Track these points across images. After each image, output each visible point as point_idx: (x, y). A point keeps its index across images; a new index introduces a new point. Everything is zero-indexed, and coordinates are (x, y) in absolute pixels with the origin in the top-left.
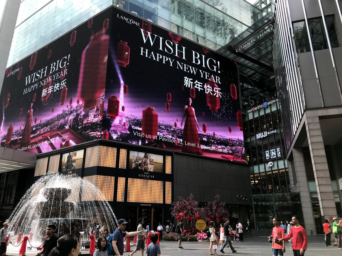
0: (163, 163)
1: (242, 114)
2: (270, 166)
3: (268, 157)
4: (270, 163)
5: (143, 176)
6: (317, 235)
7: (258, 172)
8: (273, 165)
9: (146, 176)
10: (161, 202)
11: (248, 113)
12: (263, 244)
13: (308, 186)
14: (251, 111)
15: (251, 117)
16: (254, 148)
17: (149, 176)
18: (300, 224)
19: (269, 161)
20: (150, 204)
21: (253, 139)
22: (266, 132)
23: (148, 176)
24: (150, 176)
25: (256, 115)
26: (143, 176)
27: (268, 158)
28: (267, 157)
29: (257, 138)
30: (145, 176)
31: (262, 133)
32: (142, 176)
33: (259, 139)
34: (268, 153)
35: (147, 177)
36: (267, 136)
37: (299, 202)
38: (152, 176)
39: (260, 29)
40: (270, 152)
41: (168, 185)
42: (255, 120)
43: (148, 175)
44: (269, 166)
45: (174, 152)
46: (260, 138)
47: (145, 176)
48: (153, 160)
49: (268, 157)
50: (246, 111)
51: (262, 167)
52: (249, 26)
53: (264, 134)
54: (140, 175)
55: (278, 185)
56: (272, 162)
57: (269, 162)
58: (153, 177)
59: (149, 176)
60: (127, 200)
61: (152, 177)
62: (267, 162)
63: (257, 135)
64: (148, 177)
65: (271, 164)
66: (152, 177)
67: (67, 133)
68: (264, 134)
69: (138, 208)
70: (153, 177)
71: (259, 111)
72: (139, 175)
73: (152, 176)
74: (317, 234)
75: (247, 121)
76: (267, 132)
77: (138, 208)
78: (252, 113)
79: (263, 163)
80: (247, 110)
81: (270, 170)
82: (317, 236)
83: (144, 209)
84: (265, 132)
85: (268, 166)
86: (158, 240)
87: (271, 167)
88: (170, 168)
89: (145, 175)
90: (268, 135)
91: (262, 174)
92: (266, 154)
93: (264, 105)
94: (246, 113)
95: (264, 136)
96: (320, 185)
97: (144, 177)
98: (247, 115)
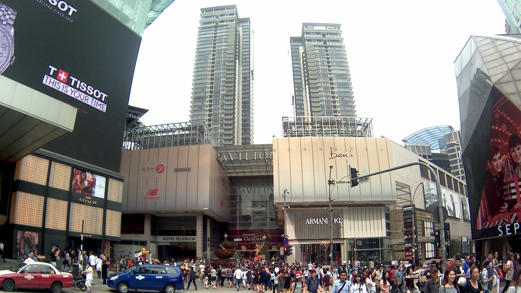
0: (73, 130)
5: (85, 201)
9: (88, 201)
10: (100, 232)
17: (90, 201)
18: (279, 229)
20: (90, 234)
23: (89, 201)
24: (91, 202)
26: (85, 201)
32: (83, 200)
38: (94, 202)
39: (240, 147)
47: (86, 201)
48: (451, 127)
52: (109, 199)
54: (81, 200)
58: (96, 204)
59: (90, 201)
60: (44, 226)
66: (94, 203)
70: (69, 19)
72: (80, 200)
73: (94, 202)
83: (254, 279)
86: (426, 283)
88: (45, 170)
97: (86, 202)
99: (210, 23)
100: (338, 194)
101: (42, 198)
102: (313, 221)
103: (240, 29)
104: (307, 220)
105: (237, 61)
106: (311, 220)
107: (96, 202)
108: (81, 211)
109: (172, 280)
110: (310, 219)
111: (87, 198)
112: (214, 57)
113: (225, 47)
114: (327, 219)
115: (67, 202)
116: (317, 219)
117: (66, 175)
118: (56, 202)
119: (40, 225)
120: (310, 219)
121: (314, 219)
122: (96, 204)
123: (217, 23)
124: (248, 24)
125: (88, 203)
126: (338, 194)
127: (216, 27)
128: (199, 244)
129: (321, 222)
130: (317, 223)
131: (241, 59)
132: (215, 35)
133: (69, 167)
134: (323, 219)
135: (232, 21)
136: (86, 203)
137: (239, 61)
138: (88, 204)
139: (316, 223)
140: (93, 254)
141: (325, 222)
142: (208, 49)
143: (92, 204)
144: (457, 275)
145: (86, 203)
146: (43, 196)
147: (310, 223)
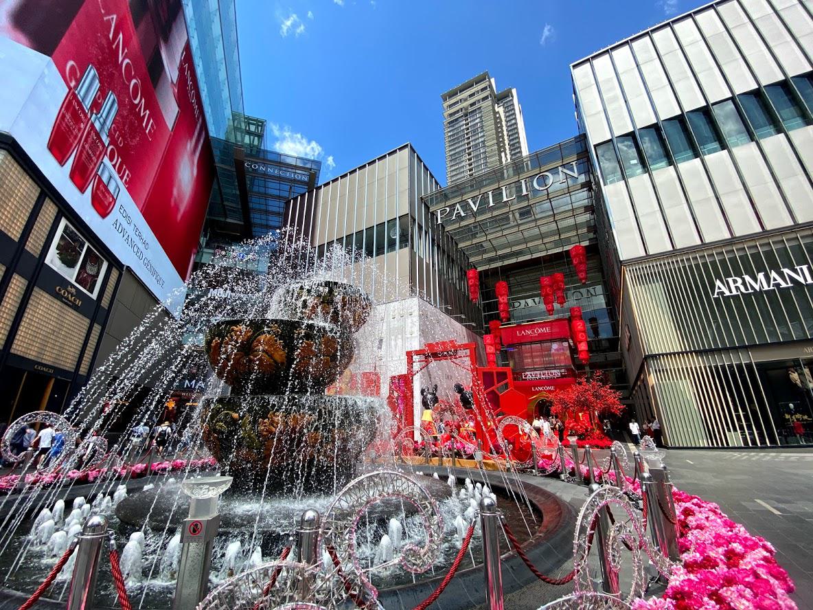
5: (64, 293)
9: (70, 295)
24: (74, 300)
26: (64, 293)
32: (63, 291)
72: (58, 288)
97: (65, 298)
99: (458, 112)
102: (744, 283)
103: (501, 110)
104: (718, 283)
105: (503, 154)
106: (735, 282)
107: (80, 303)
110: (730, 280)
112: (470, 157)
113: (483, 139)
114: (805, 268)
116: (761, 276)
117: (19, 209)
120: (730, 280)
121: (747, 278)
123: (466, 109)
124: (511, 98)
125: (67, 299)
127: (466, 115)
129: (780, 280)
130: (766, 288)
131: (508, 152)
132: (467, 126)
133: (54, 207)
134: (786, 271)
135: (486, 98)
137: (506, 155)
139: (757, 288)
140: (125, 499)
141: (801, 280)
142: (461, 149)
143: (73, 303)
147: (734, 292)
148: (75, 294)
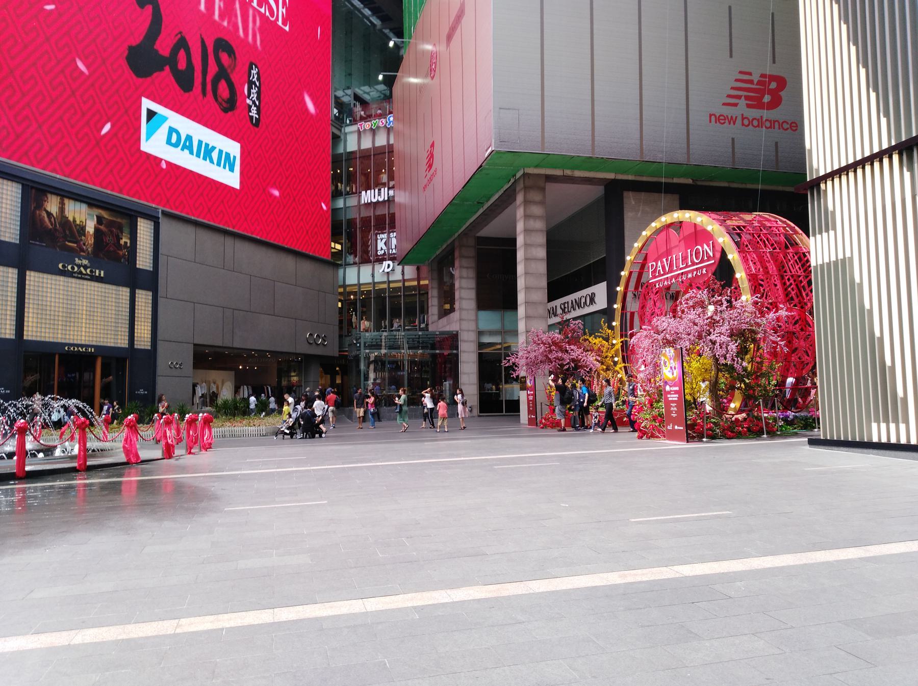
1: (333, 133)
2: (387, 270)
3: (382, 249)
4: (386, 263)
5: (73, 268)
6: (481, 414)
7: (356, 282)
8: (393, 270)
9: (82, 269)
10: (123, 342)
11: (346, 134)
12: (342, 444)
13: (477, 320)
14: (354, 128)
15: (351, 144)
16: (351, 223)
17: (88, 271)
19: (385, 260)
20: (92, 346)
21: (352, 201)
22: (386, 189)
24: (91, 271)
25: (367, 144)
26: (73, 268)
27: (383, 252)
28: (379, 248)
29: (363, 202)
30: (76, 269)
31: (377, 191)
33: (368, 205)
34: (384, 241)
35: (84, 272)
36: (386, 199)
37: (455, 352)
38: (97, 271)
40: (389, 237)
41: (144, 298)
42: (365, 155)
43: (85, 267)
44: (383, 271)
45: (163, 211)
46: (369, 201)
47: (76, 269)
49: (382, 249)
50: (342, 127)
51: (366, 270)
53: (379, 194)
54: (63, 266)
55: (399, 316)
56: (390, 262)
57: (384, 262)
58: (102, 275)
61: (97, 274)
62: (380, 260)
63: (363, 193)
64: (87, 274)
65: (389, 266)
66: (97, 274)
67: (626, 243)
68: (379, 194)
69: (57, 357)
70: (100, 274)
71: (373, 132)
72: (60, 266)
73: (97, 271)
74: (479, 413)
75: (343, 153)
76: (388, 191)
77: (57, 357)
78: (355, 136)
79: (371, 262)
80: (344, 125)
81: (385, 279)
82: (479, 416)
84: (382, 189)
85: (381, 271)
87: (388, 273)
89: (79, 266)
90: (388, 197)
91: (363, 288)
92: (379, 241)
93: (389, 119)
94: (340, 130)
95: (381, 199)
96: (527, 317)
97: (75, 273)
98: (342, 137)
100: (777, 156)
101: (125, 292)
107: (102, 273)
108: (99, 298)
109: (106, 492)
111: (77, 261)
115: (128, 290)
118: (78, 286)
119: (28, 335)
122: (102, 275)
125: (81, 273)
126: (777, 156)
128: (468, 362)
136: (76, 275)
138: (81, 277)
144: (393, 329)
145: (76, 275)
146: (13, 266)
148: (89, 265)
